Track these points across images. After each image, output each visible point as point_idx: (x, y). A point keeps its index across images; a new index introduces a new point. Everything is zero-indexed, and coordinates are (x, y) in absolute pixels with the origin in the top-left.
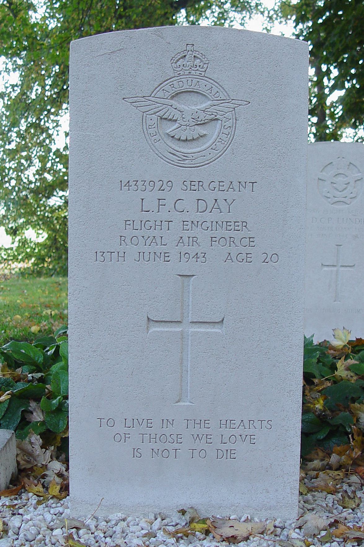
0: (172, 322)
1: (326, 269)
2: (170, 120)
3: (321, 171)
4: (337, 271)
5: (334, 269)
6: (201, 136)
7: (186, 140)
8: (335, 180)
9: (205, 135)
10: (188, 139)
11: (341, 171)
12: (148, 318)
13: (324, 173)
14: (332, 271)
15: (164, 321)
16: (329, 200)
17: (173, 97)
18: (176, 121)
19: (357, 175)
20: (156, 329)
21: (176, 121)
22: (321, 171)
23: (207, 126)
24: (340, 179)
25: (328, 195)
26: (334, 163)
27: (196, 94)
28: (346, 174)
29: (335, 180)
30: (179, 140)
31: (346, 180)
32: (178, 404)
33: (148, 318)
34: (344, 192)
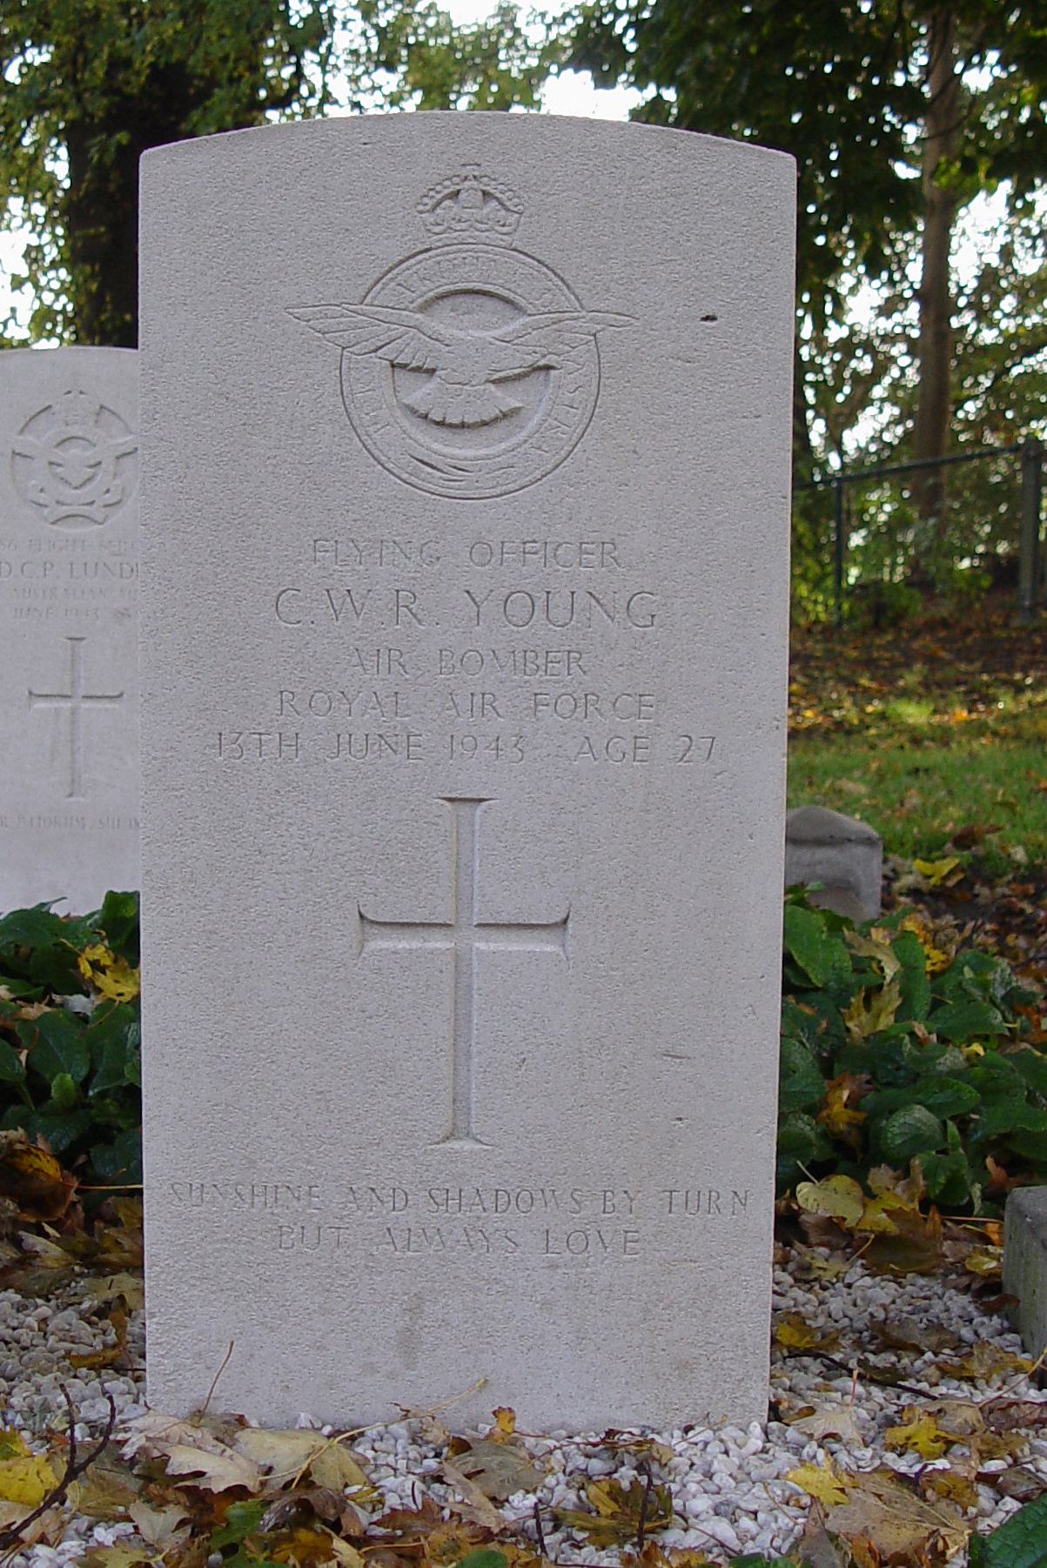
0: (519, 926)
1: (41, 705)
2: (418, 369)
3: (22, 432)
4: (73, 712)
5: (66, 705)
6: (505, 415)
7: (426, 417)
8: (58, 455)
9: (515, 411)
10: (448, 421)
11: (75, 430)
12: (362, 916)
13: (29, 437)
14: (57, 712)
15: (436, 925)
16: (46, 511)
17: (425, 307)
18: (432, 371)
19: (120, 441)
20: (383, 943)
21: (432, 371)
22: (22, 432)
23: (519, 386)
24: (75, 451)
25: (42, 498)
26: (56, 408)
27: (500, 305)
28: (88, 437)
29: (58, 455)
30: (440, 424)
31: (91, 455)
32: (448, 1145)
33: (362, 916)
34: (85, 489)
